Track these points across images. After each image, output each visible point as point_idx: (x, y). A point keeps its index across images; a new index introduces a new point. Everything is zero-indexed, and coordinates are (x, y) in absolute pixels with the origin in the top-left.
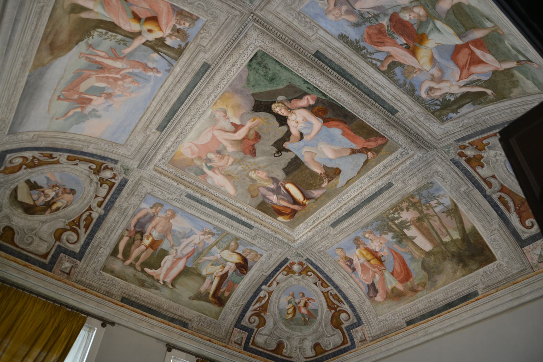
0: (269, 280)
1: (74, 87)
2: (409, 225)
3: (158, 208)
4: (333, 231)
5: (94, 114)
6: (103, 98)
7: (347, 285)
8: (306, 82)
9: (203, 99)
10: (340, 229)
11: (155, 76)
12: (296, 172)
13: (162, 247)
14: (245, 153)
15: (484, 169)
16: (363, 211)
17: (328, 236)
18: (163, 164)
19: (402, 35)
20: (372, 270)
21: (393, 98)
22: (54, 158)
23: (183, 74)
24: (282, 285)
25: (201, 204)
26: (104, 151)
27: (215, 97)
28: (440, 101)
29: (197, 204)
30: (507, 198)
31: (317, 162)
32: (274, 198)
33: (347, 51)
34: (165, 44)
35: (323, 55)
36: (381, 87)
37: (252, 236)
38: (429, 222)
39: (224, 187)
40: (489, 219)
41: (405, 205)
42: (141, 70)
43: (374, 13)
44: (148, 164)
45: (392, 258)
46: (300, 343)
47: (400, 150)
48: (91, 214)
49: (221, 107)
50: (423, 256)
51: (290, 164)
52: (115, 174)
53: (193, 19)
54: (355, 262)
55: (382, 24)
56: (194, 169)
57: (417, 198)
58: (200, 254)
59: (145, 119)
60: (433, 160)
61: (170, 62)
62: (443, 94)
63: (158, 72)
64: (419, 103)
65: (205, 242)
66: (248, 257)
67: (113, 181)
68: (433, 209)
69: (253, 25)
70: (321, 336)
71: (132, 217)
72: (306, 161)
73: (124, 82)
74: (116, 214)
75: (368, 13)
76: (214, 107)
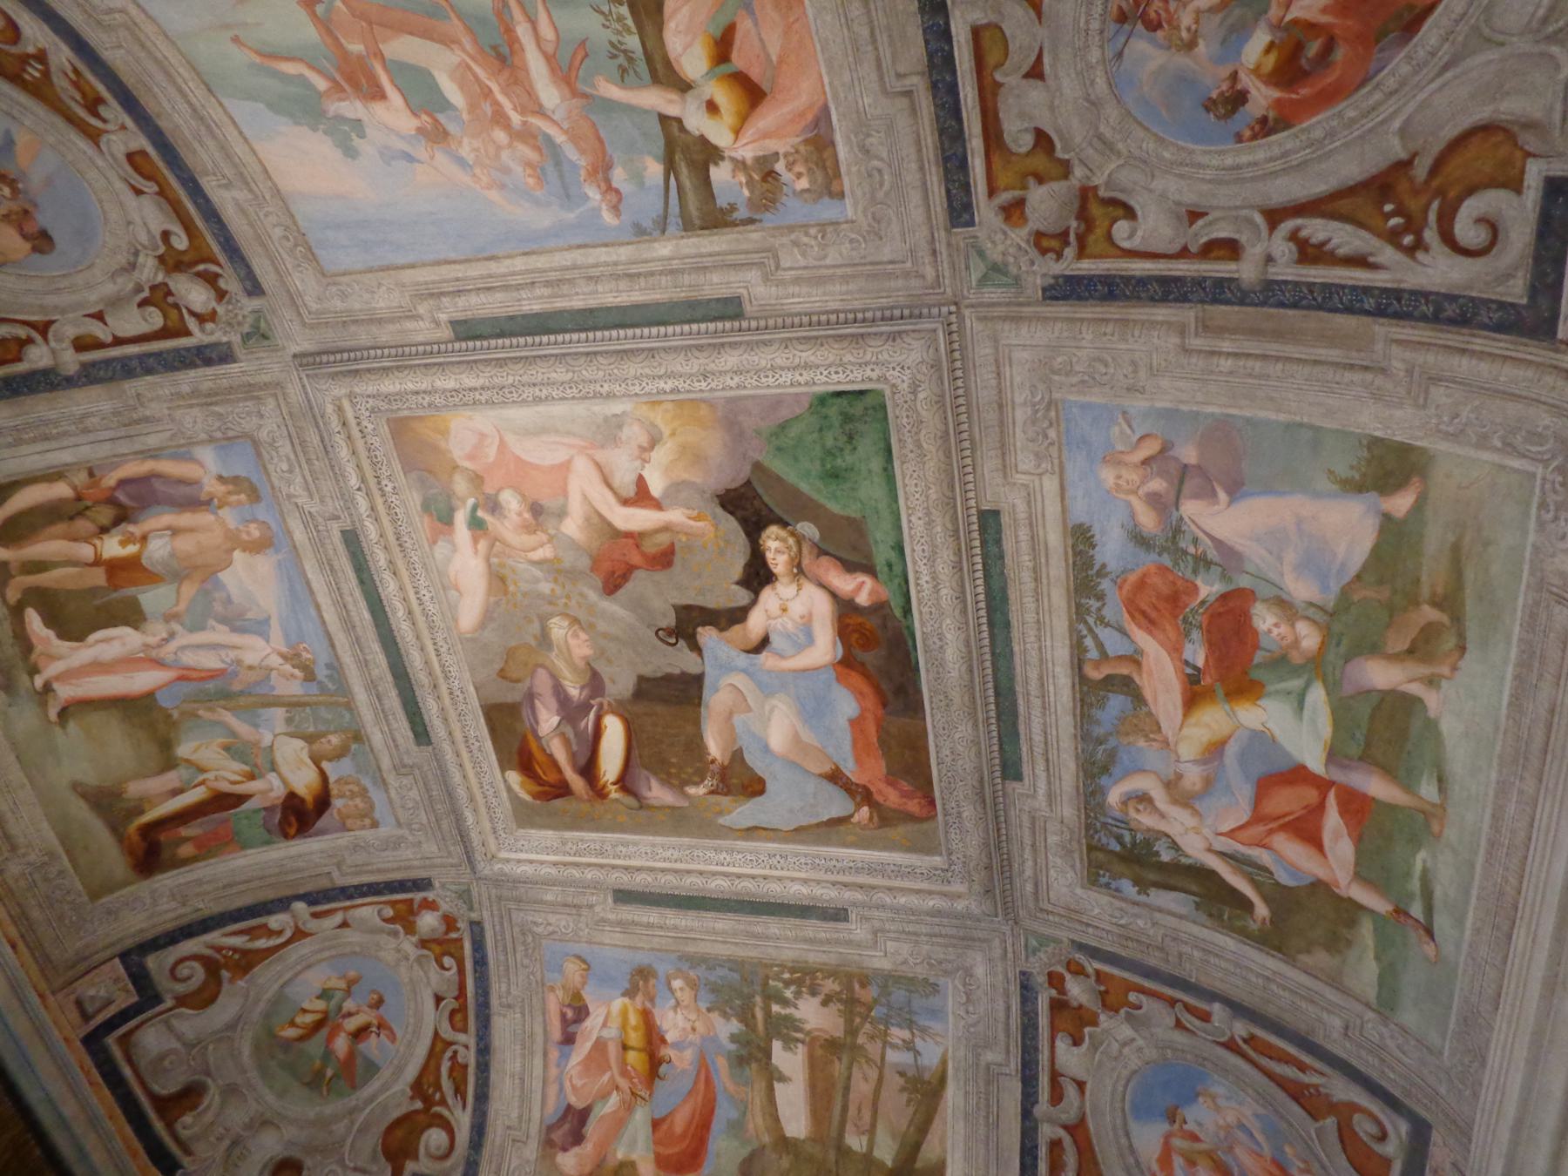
0: (334, 899)
1: (381, 25)
3: (239, 493)
4: (606, 908)
5: (346, 135)
7: (518, 1065)
8: (900, 548)
9: (647, 371)
10: (630, 917)
11: (600, 209)
12: (660, 709)
13: (139, 597)
14: (594, 568)
15: (1075, 1050)
16: (724, 923)
17: (584, 912)
19: (1211, 645)
20: (612, 1076)
21: (1043, 745)
22: (97, 115)
23: (661, 273)
24: (350, 936)
25: (362, 582)
27: (675, 391)
28: (1134, 838)
29: (351, 574)
31: (732, 728)
32: (548, 720)
33: (1058, 570)
34: (708, 170)
35: (999, 531)
36: (1044, 702)
38: (850, 1068)
39: (461, 594)
41: (830, 986)
42: (583, 163)
43: (1205, 553)
44: (337, 374)
45: (687, 1084)
46: (249, 1127)
47: (937, 860)
48: (30, 341)
49: (659, 421)
50: (766, 1139)
52: (214, 314)
53: (829, 184)
54: (588, 1023)
55: (1196, 589)
56: (434, 491)
57: (872, 992)
59: (453, 275)
60: (985, 941)
61: (666, 218)
63: (616, 209)
64: (1087, 802)
65: (268, 677)
67: (192, 324)
68: (884, 1048)
69: (935, 331)
71: (142, 452)
73: (510, 146)
74: (106, 406)
75: (1195, 541)
76: (645, 407)
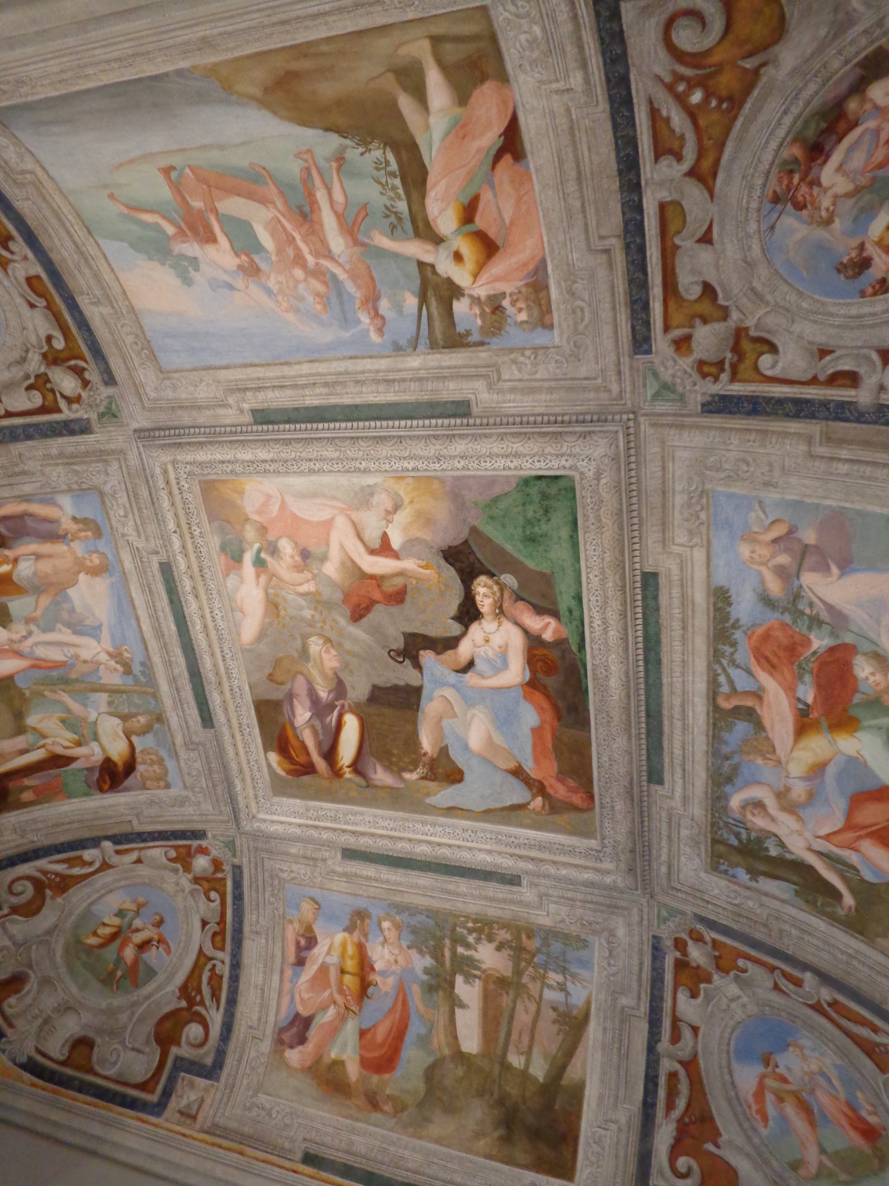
1: (218, 188)
2: (475, 976)
3: (85, 531)
4: (336, 863)
6: (237, 261)
8: (579, 598)
10: (354, 870)
11: (368, 331)
12: (387, 711)
16: (425, 880)
17: (319, 864)
18: (189, 474)
19: (819, 687)
20: (331, 994)
23: (411, 380)
24: (143, 871)
25: (171, 602)
26: (115, 342)
28: (749, 835)
30: (684, 1087)
32: (302, 715)
33: (701, 621)
35: (657, 589)
36: (684, 724)
37: (191, 738)
38: (514, 1002)
40: (621, 1094)
41: (504, 935)
42: (358, 295)
43: (818, 614)
44: (165, 445)
45: (388, 1003)
46: (57, 1010)
47: (593, 843)
49: (402, 493)
50: (447, 1052)
51: (395, 689)
52: (79, 398)
54: (316, 951)
55: (809, 642)
57: (535, 944)
58: (65, 682)
59: (255, 375)
62: (769, 832)
63: (380, 331)
65: (97, 670)
66: (140, 768)
67: (63, 404)
69: (617, 432)
70: (112, 1033)
71: (19, 497)
72: (427, 710)
73: (305, 280)
75: (811, 605)
76: (392, 481)
